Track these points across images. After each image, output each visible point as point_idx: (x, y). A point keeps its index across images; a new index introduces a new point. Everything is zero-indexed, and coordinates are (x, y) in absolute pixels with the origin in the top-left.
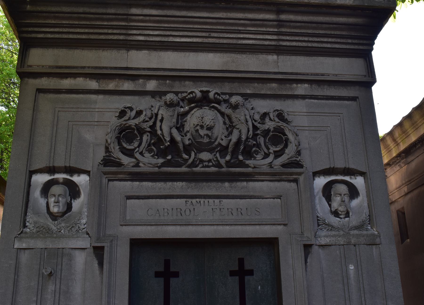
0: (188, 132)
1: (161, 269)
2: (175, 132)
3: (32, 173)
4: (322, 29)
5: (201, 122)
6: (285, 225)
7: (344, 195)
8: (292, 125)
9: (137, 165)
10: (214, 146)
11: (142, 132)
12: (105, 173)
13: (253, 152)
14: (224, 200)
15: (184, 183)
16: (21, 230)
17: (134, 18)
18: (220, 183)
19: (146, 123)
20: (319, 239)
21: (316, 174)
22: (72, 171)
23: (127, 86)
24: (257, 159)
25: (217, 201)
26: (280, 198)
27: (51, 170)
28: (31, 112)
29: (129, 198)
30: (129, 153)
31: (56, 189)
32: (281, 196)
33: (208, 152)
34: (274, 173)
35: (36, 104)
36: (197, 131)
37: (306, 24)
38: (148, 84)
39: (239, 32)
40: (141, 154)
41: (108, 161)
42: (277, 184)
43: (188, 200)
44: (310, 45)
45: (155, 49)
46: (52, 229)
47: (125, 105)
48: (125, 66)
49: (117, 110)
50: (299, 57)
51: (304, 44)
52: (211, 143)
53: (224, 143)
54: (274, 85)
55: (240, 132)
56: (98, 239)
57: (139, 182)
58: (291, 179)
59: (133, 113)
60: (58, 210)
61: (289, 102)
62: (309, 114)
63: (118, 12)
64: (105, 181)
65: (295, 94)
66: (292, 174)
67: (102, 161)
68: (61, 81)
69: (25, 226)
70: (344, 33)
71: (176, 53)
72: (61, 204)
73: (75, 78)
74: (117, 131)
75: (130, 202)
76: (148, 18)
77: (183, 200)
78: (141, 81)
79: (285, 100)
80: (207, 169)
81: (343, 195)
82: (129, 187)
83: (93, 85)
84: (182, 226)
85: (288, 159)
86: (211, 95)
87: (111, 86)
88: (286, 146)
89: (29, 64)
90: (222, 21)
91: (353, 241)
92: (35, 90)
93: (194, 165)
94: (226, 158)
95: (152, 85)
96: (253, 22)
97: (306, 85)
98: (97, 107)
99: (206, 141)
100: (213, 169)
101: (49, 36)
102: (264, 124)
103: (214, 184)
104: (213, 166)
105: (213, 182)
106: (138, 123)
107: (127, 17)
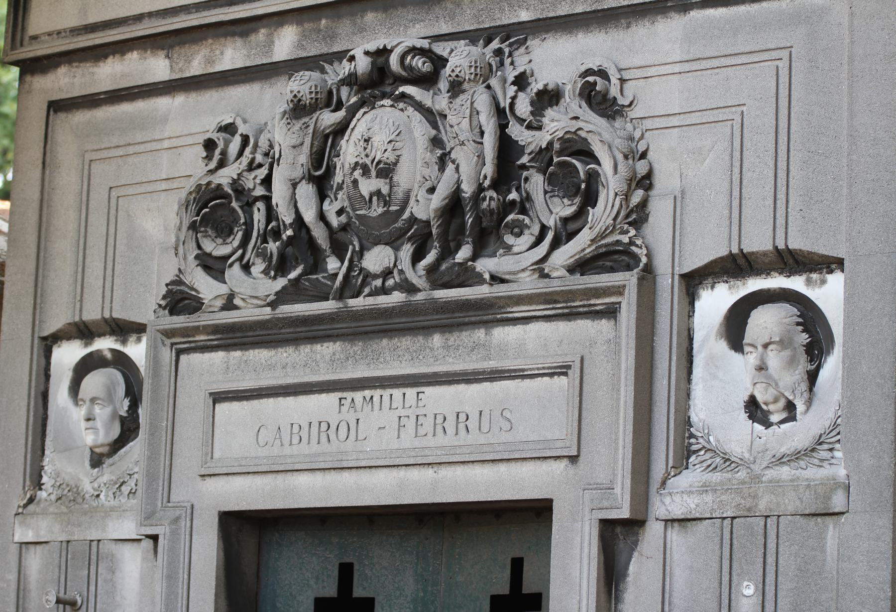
0: (340, 187)
3: (49, 342)
5: (363, 156)
6: (573, 459)
7: (766, 346)
8: (632, 115)
9: (229, 305)
12: (168, 333)
14: (429, 391)
15: (338, 343)
16: (28, 496)
18: (421, 338)
20: (668, 500)
21: (693, 282)
23: (231, 55)
24: (516, 249)
25: (411, 392)
26: (565, 374)
27: (84, 331)
29: (218, 398)
30: (214, 267)
31: (94, 382)
32: (569, 367)
33: (386, 244)
34: (546, 293)
35: (48, 147)
36: (355, 182)
38: (277, 42)
40: (246, 268)
41: (180, 300)
42: (562, 327)
43: (345, 394)
46: (83, 490)
47: (219, 120)
52: (390, 217)
53: (421, 215)
56: (148, 517)
57: (241, 350)
58: (598, 308)
59: (235, 144)
60: (94, 440)
62: (687, 67)
64: (167, 355)
67: (164, 297)
68: (96, 70)
72: (99, 424)
74: (193, 208)
75: (222, 408)
79: (628, 26)
80: (383, 301)
81: (760, 349)
82: (211, 368)
83: (157, 67)
84: (327, 471)
85: (592, 241)
87: (196, 63)
88: (590, 199)
91: (763, 505)
92: (45, 107)
93: (350, 287)
94: (457, 256)
98: (166, 135)
99: (375, 214)
100: (397, 297)
102: (539, 128)
103: (406, 342)
104: (397, 287)
105: (404, 336)
106: (235, 177)
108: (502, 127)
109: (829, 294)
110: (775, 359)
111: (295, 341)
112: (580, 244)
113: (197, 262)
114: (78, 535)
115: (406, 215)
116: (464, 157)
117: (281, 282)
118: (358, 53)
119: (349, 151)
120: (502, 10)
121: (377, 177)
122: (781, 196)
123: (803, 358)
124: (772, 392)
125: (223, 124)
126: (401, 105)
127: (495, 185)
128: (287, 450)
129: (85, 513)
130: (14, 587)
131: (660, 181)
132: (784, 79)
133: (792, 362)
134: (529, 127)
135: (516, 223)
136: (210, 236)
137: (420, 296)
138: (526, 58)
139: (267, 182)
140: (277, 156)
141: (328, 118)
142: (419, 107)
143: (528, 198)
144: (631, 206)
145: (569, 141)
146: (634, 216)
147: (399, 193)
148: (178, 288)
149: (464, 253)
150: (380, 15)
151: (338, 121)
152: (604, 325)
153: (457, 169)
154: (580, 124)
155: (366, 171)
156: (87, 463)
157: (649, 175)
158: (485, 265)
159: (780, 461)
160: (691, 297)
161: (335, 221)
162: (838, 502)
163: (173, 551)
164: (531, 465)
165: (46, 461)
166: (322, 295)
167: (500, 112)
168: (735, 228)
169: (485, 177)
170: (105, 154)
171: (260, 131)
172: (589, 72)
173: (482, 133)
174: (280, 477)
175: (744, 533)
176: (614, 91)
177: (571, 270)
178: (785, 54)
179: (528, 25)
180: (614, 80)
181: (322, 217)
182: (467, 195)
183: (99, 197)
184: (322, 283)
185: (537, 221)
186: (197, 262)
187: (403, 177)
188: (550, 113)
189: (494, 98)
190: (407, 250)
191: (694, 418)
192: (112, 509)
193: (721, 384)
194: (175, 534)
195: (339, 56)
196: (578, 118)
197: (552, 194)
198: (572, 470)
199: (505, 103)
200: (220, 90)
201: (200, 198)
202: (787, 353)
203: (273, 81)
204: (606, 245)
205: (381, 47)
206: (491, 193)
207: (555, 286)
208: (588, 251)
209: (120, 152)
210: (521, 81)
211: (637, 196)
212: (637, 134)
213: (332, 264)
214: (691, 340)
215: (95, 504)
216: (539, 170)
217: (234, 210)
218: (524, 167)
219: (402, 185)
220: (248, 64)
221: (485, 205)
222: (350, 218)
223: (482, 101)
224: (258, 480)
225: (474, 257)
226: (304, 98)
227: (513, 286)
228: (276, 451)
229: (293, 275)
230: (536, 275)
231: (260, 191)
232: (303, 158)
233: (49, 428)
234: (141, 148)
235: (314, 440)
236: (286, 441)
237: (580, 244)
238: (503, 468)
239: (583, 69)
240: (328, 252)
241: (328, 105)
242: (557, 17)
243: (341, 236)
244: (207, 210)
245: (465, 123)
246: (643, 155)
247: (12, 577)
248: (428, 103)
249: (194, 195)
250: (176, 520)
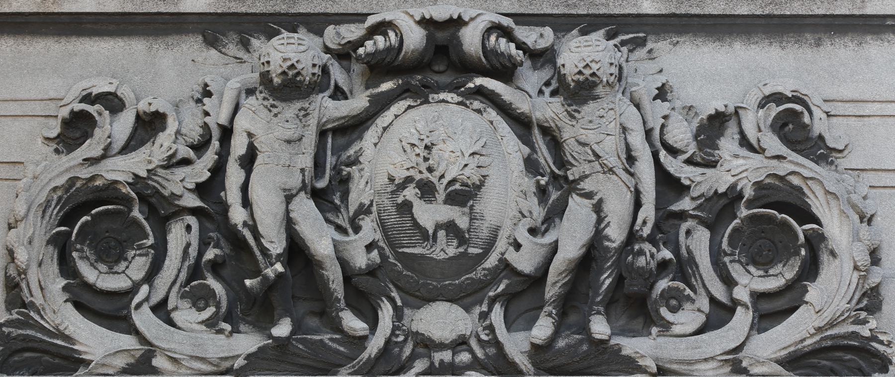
0: (364, 210)
5: (423, 168)
10: (479, 273)
11: (162, 211)
19: (181, 172)
24: (676, 329)
30: (110, 311)
36: (406, 208)
40: (161, 309)
47: (85, 84)
55: (598, 208)
59: (122, 127)
74: (54, 211)
102: (712, 165)
106: (144, 174)
113: (66, 296)
115: (491, 261)
121: (446, 202)
125: (95, 91)
126: (477, 104)
127: (651, 239)
134: (689, 162)
135: (673, 293)
136: (87, 258)
138: (652, 66)
143: (692, 261)
144: (867, 287)
145: (769, 187)
146: (865, 302)
148: (20, 332)
151: (355, 113)
153: (598, 208)
166: (321, 366)
169: (644, 223)
179: (651, 20)
182: (614, 245)
184: (330, 348)
185: (704, 293)
186: (66, 296)
196: (785, 158)
197: (732, 258)
199: (656, 123)
200: (63, 40)
201: (69, 198)
203: (170, 40)
204: (832, 337)
205: (455, 17)
208: (809, 342)
213: (353, 323)
216: (702, 222)
217: (135, 222)
219: (488, 218)
220: (127, 10)
222: (382, 255)
226: (304, 72)
230: (728, 369)
231: (192, 201)
234: (29, 109)
239: (767, 91)
240: (342, 304)
242: (704, 16)
243: (364, 283)
244: (89, 218)
249: (59, 193)
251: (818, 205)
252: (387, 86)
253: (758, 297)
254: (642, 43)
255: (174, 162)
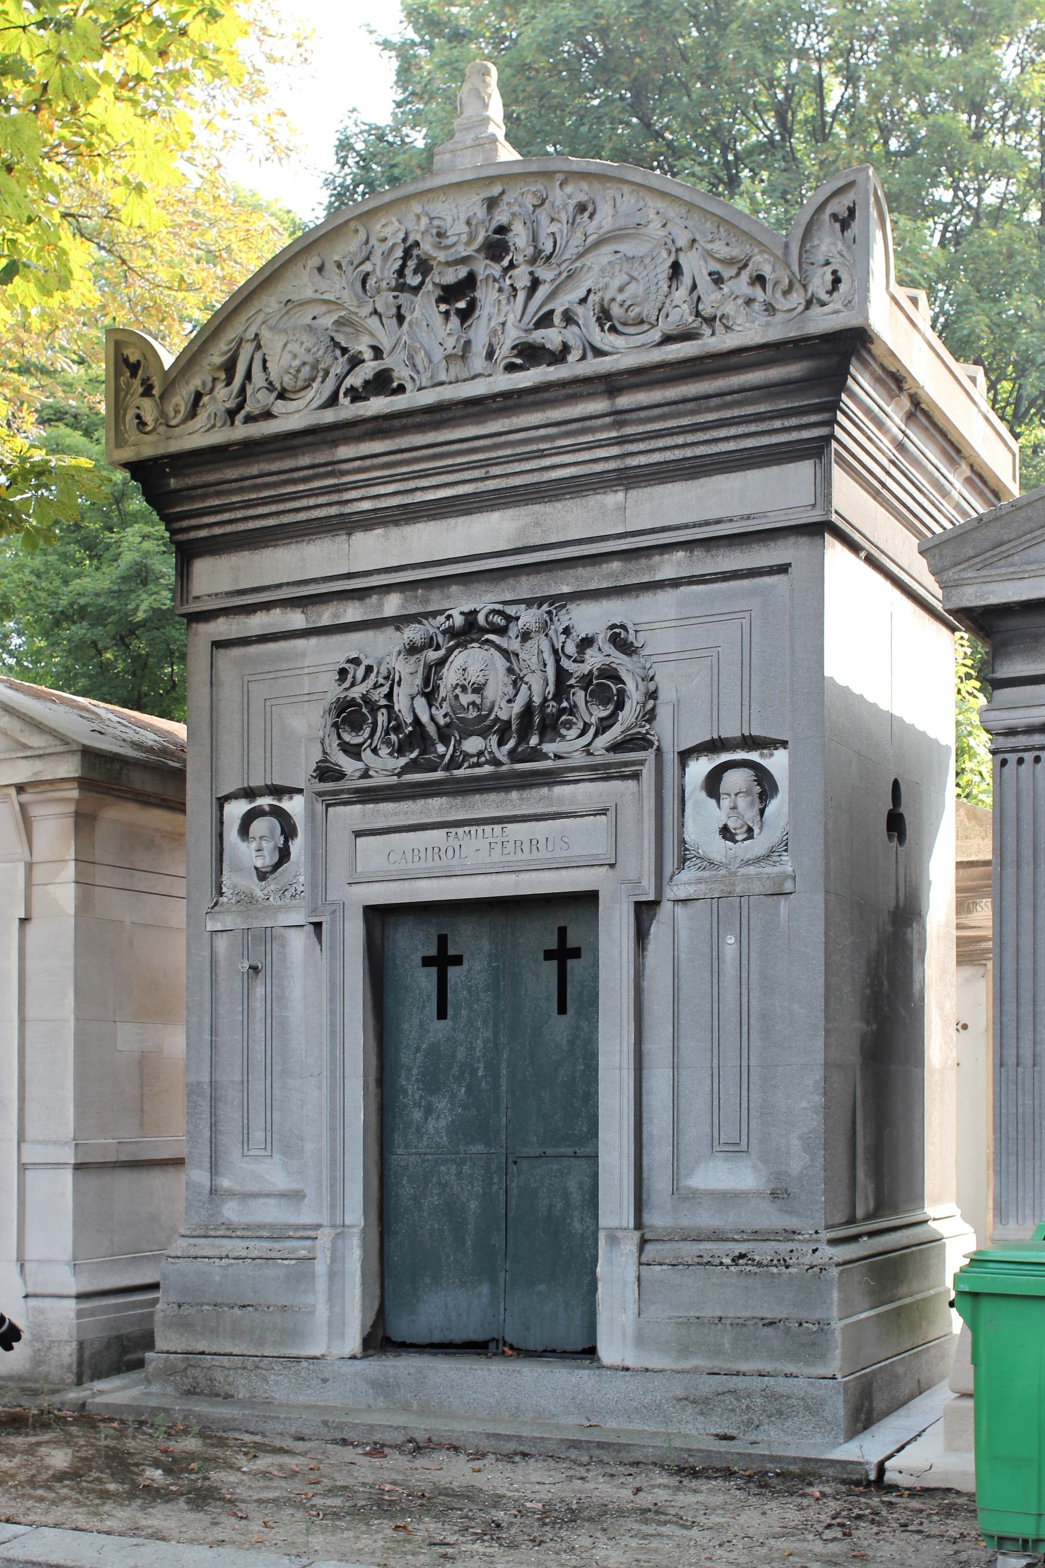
0: (444, 699)
1: (433, 951)
2: (421, 703)
3: (222, 802)
4: (710, 410)
6: (612, 866)
8: (643, 653)
9: (366, 775)
10: (487, 723)
11: (374, 708)
12: (320, 794)
13: (572, 718)
17: (345, 466)
19: (379, 690)
21: (685, 756)
22: (278, 791)
23: (352, 612)
25: (497, 828)
27: (249, 793)
28: (207, 689)
29: (358, 834)
30: (353, 751)
31: (259, 826)
36: (457, 697)
37: (674, 407)
39: (541, 454)
40: (375, 751)
41: (326, 772)
42: (601, 785)
44: (689, 453)
45: (397, 523)
48: (345, 571)
49: (332, 667)
50: (670, 485)
51: (678, 454)
53: (504, 716)
54: (616, 565)
55: (530, 688)
56: (314, 911)
59: (361, 672)
61: (646, 599)
62: (680, 623)
63: (317, 461)
64: (320, 807)
65: (657, 578)
66: (626, 764)
69: (221, 894)
70: (762, 408)
71: (432, 523)
72: (266, 853)
73: (268, 610)
74: (334, 712)
76: (368, 462)
77: (443, 832)
78: (374, 599)
80: (478, 771)
82: (355, 815)
83: (297, 620)
86: (481, 619)
87: (326, 616)
88: (620, 706)
89: (195, 594)
90: (503, 439)
91: (738, 890)
93: (454, 764)
95: (392, 605)
96: (564, 428)
97: (681, 554)
100: (487, 769)
101: (218, 531)
102: (583, 662)
103: (493, 796)
104: (487, 762)
107: (333, 468)
108: (558, 661)
109: (777, 762)
110: (742, 802)
111: (414, 797)
112: (614, 734)
114: (255, 924)
115: (492, 717)
116: (535, 681)
117: (403, 761)
118: (455, 613)
119: (450, 676)
120: (549, 585)
122: (746, 703)
123: (757, 801)
124: (740, 822)
128: (410, 866)
129: (260, 910)
130: (208, 960)
131: (662, 696)
132: (746, 630)
133: (752, 804)
134: (575, 661)
137: (504, 768)
138: (567, 617)
139: (389, 696)
140: (397, 679)
141: (433, 655)
142: (498, 648)
143: (576, 705)
147: (487, 703)
149: (534, 741)
150: (461, 588)
152: (631, 784)
153: (530, 688)
154: (612, 659)
155: (464, 689)
156: (255, 878)
157: (655, 691)
158: (548, 748)
159: (748, 863)
160: (683, 766)
161: (442, 722)
162: (788, 886)
163: (333, 932)
164: (582, 871)
165: (224, 878)
167: (555, 652)
168: (715, 723)
170: (259, 677)
171: (380, 664)
172: (613, 626)
173: (545, 665)
174: (407, 883)
175: (726, 905)
176: (631, 638)
177: (608, 750)
178: (746, 615)
180: (631, 631)
181: (432, 718)
183: (257, 706)
187: (490, 693)
188: (589, 652)
189: (553, 646)
190: (494, 739)
191: (687, 838)
192: (280, 907)
193: (703, 820)
194: (333, 921)
195: (434, 614)
198: (611, 872)
202: (749, 799)
206: (552, 703)
207: (599, 760)
209: (272, 676)
210: (567, 631)
211: (650, 704)
212: (648, 665)
213: (441, 749)
214: (683, 791)
215: (266, 904)
216: (581, 688)
218: (572, 686)
221: (549, 710)
223: (545, 645)
224: (391, 885)
225: (540, 744)
227: (570, 761)
228: (402, 866)
229: (413, 755)
231: (383, 702)
232: (419, 681)
233: (225, 857)
234: (288, 673)
235: (430, 858)
236: (410, 859)
237: (614, 734)
238: (564, 872)
241: (430, 646)
243: (446, 730)
245: (534, 659)
246: (652, 679)
247: (207, 953)
248: (505, 645)
250: (334, 911)
251: (624, 675)
252: (452, 643)
253: (601, 720)
254: (564, 606)
255: (376, 686)
